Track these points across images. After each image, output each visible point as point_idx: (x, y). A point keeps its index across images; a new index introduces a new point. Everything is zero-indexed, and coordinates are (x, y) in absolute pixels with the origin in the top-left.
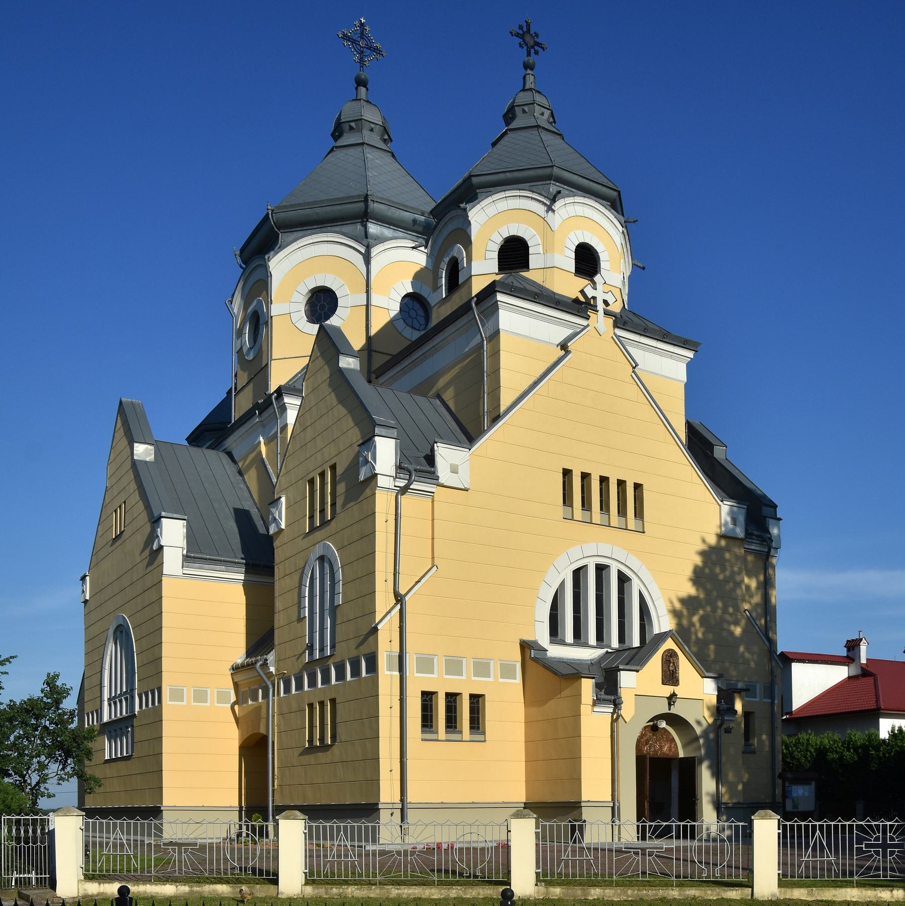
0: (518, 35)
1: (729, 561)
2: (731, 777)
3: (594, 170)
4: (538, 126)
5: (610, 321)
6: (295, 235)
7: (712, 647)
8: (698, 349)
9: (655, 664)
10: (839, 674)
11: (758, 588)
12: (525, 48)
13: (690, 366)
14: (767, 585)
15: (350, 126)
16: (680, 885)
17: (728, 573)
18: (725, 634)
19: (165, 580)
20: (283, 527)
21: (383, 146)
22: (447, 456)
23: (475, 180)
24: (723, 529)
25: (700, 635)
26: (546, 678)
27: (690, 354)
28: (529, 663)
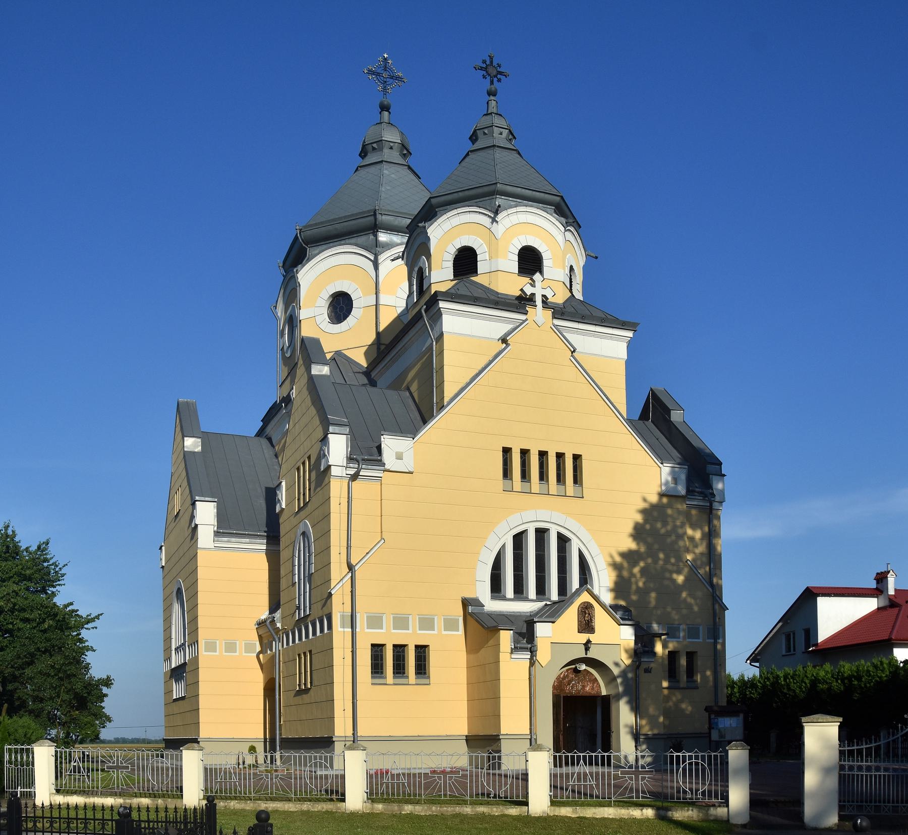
0: (481, 69)
1: (671, 516)
2: (652, 710)
5: (549, 313)
6: (320, 248)
7: (653, 595)
8: (637, 328)
9: (571, 615)
10: (870, 605)
11: (702, 539)
13: (631, 346)
14: (712, 535)
16: (473, 803)
17: (669, 528)
18: (666, 582)
19: (200, 553)
20: (284, 507)
21: (402, 161)
22: (391, 445)
24: (663, 488)
25: (641, 584)
26: (480, 627)
27: (630, 334)
28: (469, 617)
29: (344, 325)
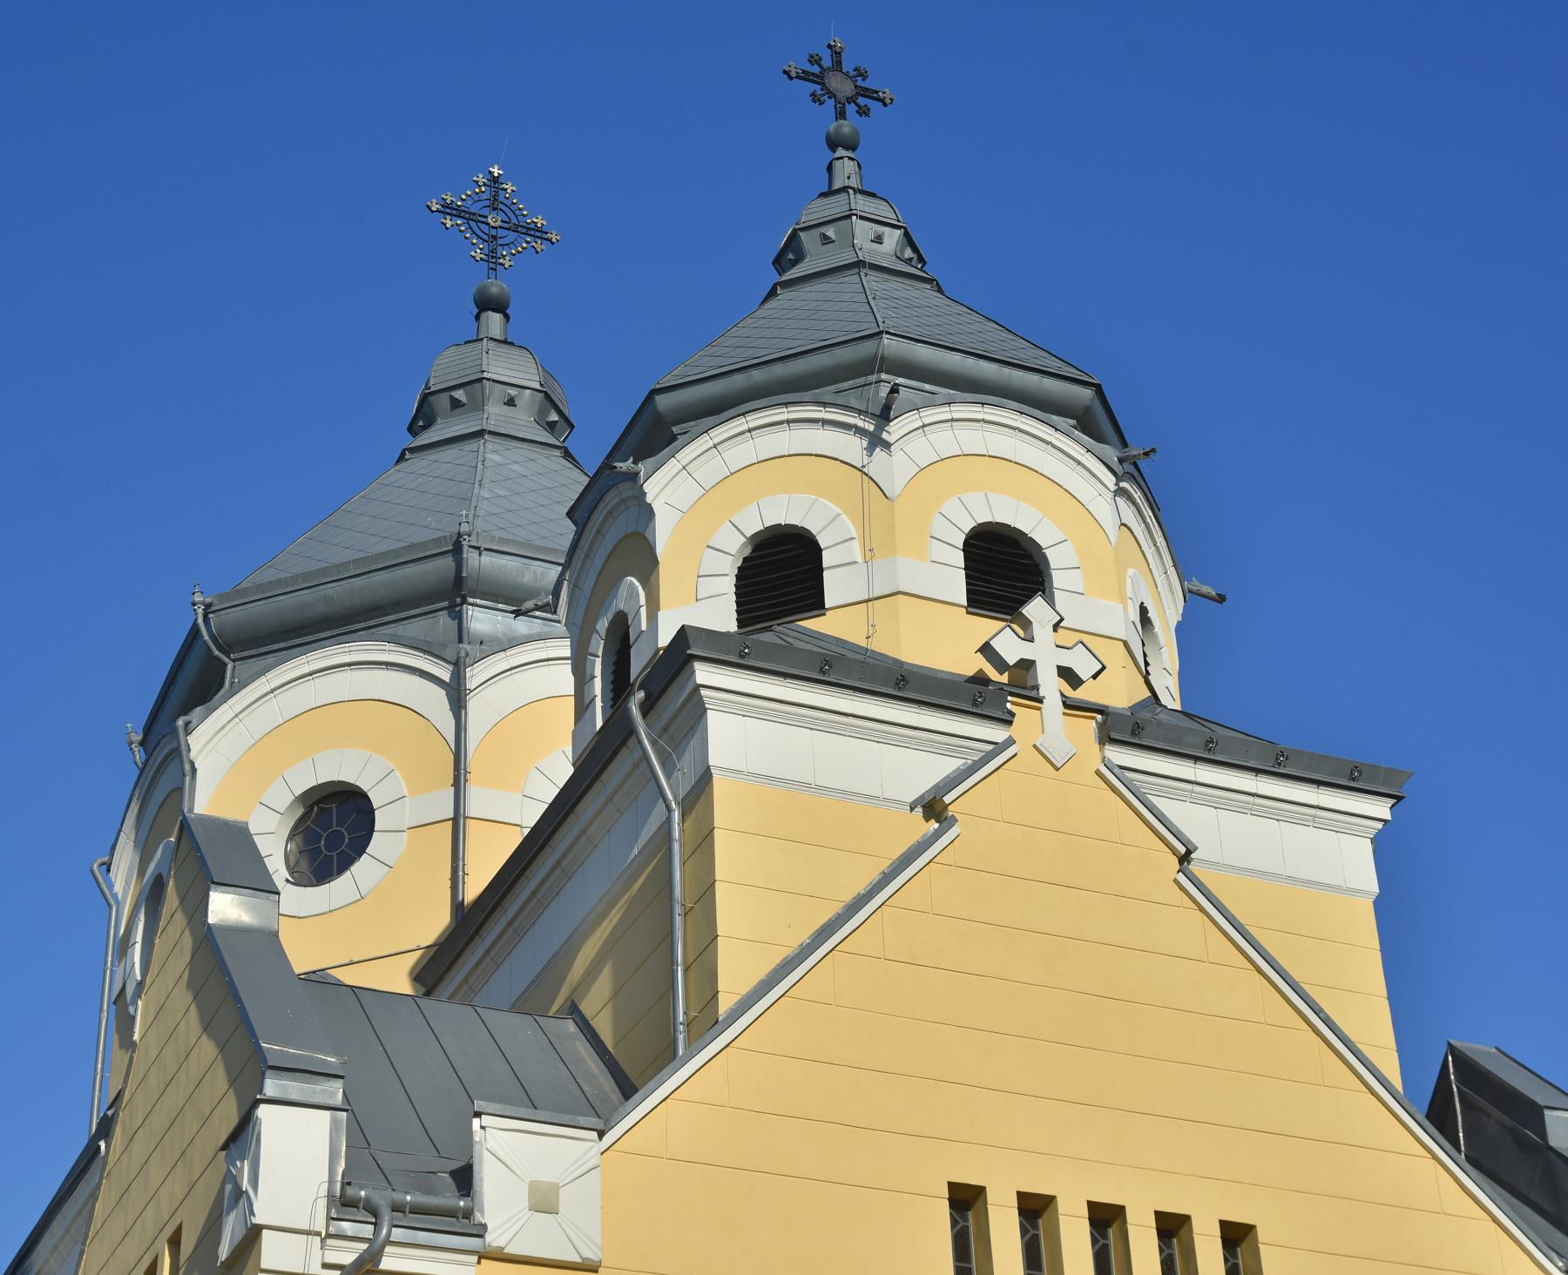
0: (805, 76)
3: (979, 318)
4: (859, 264)
5: (1088, 726)
12: (830, 103)
13: (1385, 846)
15: (452, 398)
22: (515, 1157)
23: (663, 402)
27: (1381, 809)
29: (340, 888)
